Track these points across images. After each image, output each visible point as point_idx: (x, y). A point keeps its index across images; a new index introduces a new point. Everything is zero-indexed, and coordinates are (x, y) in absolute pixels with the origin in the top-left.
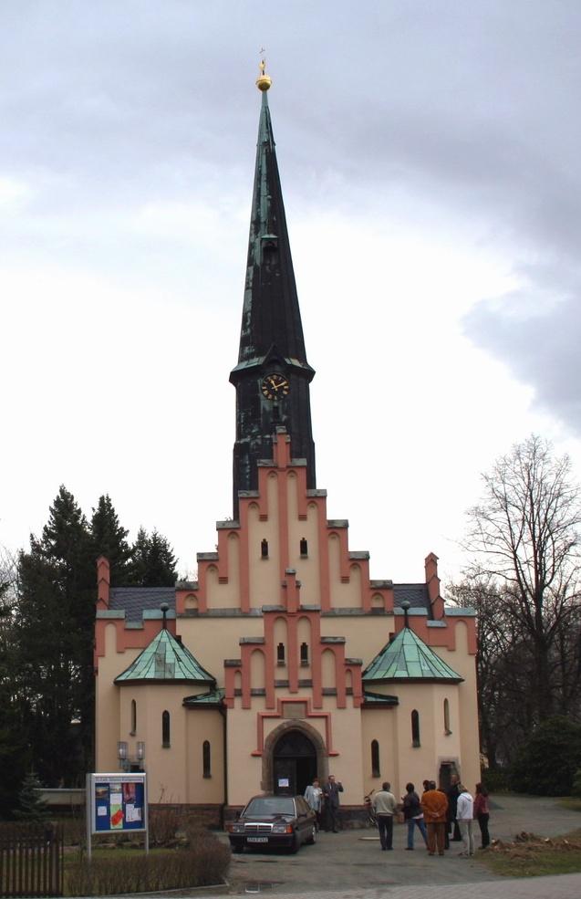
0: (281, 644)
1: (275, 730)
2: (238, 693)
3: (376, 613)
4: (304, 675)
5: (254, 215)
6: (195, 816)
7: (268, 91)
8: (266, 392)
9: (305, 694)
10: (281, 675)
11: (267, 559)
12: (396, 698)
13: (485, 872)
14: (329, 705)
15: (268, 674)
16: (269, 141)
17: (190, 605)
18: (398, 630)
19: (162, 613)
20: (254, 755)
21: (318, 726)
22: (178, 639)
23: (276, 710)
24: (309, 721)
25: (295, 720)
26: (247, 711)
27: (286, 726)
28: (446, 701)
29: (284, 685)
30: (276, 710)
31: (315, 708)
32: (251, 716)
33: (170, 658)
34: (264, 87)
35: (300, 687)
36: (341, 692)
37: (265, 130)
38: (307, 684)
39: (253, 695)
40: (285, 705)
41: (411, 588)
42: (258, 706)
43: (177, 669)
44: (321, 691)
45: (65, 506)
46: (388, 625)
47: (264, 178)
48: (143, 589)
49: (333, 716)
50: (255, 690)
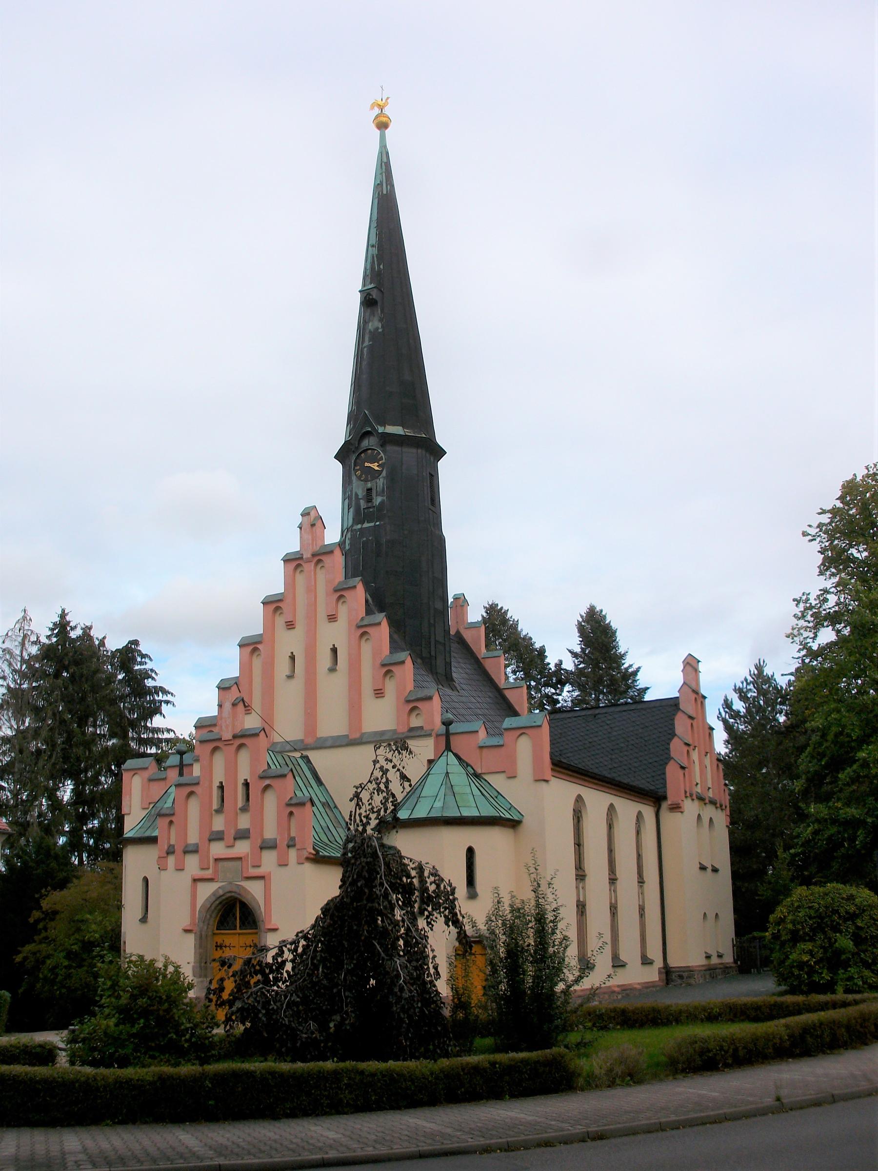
0: (221, 783)
1: (210, 897)
4: (244, 822)
7: (387, 132)
9: (242, 848)
10: (218, 823)
14: (269, 859)
20: (187, 931)
21: (255, 891)
23: (210, 871)
25: (231, 883)
27: (221, 892)
28: (470, 852)
29: (218, 837)
30: (210, 871)
31: (254, 867)
32: (185, 878)
34: (382, 126)
35: (235, 839)
36: (282, 844)
38: (243, 835)
40: (221, 864)
41: (658, 704)
42: (192, 863)
44: (259, 842)
45: (485, 607)
49: (273, 878)
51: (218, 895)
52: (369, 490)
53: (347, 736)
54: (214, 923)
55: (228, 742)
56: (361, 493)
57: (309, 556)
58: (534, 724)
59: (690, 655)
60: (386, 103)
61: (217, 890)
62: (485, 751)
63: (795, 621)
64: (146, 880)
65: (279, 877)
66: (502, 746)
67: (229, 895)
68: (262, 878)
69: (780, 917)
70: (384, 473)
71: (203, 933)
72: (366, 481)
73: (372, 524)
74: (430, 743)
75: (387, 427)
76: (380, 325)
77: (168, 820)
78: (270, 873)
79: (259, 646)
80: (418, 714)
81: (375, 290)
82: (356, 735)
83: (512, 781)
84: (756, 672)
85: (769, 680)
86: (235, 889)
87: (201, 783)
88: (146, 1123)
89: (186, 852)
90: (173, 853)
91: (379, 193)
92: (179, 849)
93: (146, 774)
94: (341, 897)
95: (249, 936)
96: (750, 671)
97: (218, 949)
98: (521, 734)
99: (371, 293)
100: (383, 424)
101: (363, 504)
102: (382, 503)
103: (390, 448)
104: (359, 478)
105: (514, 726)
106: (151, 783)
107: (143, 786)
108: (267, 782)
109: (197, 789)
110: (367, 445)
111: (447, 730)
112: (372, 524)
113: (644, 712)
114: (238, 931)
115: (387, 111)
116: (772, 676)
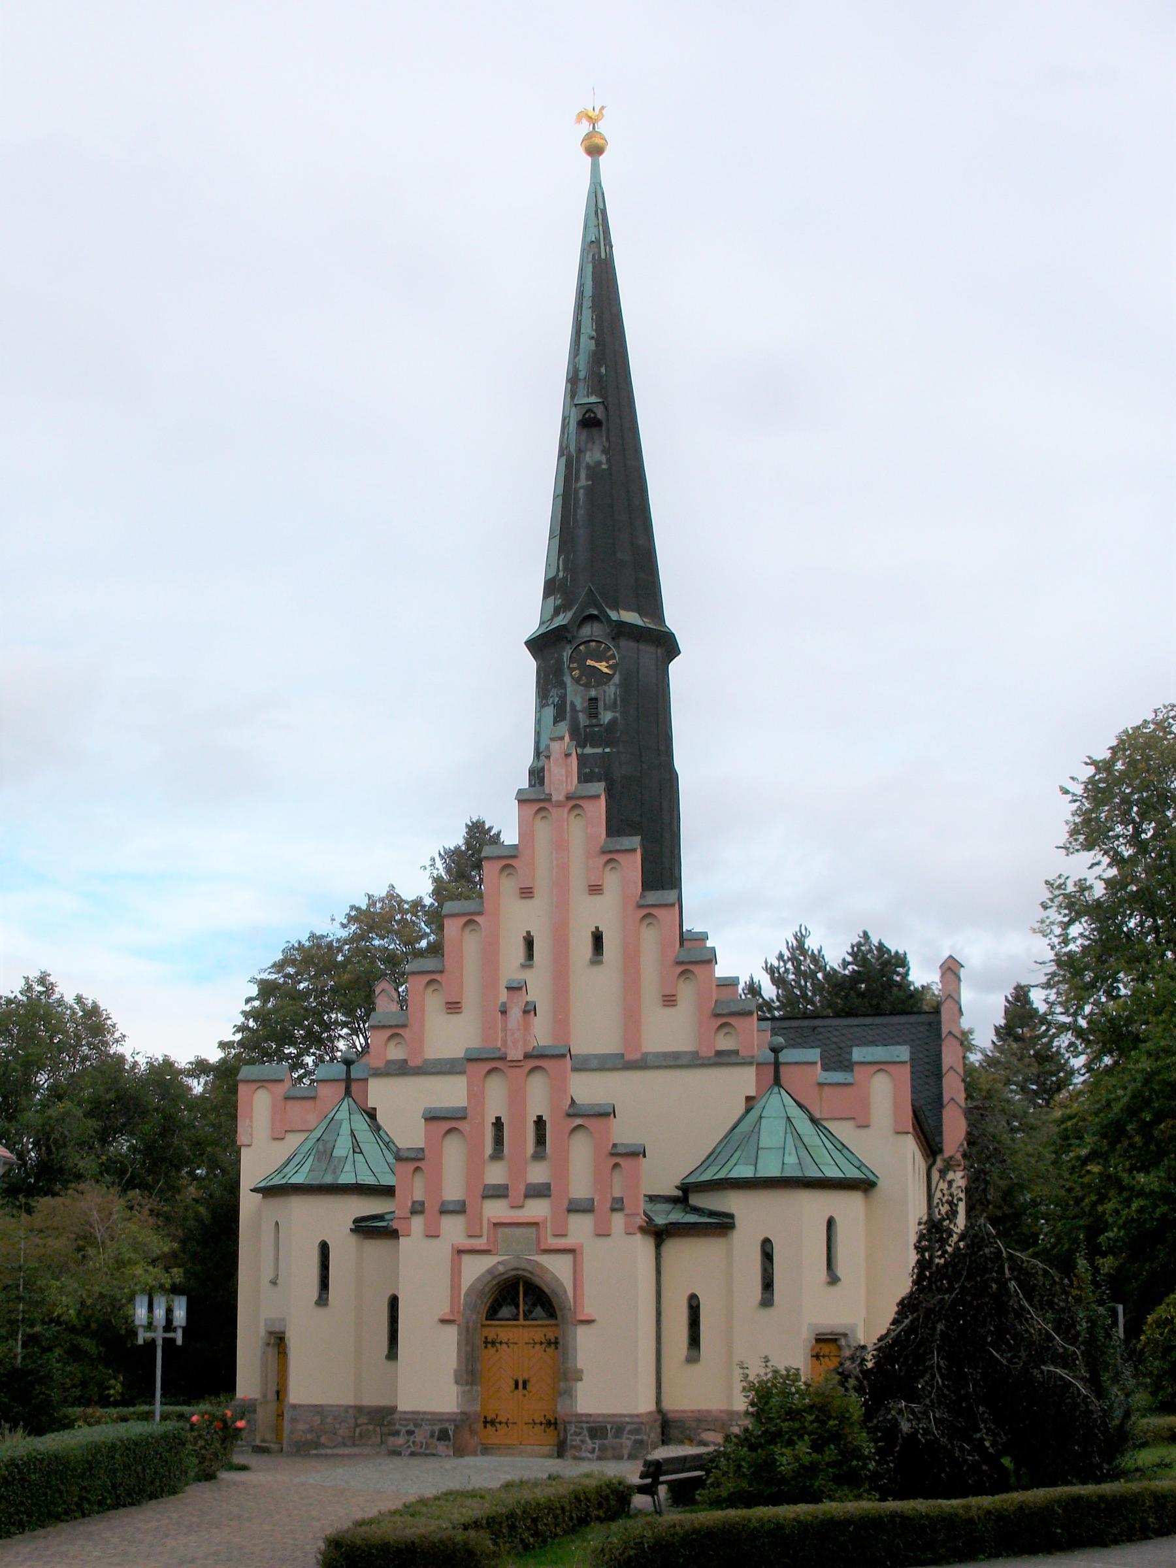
0: (498, 1119)
1: (483, 1275)
2: (417, 1209)
3: (724, 1059)
4: (538, 1174)
5: (571, 366)
6: (371, 1427)
7: (601, 158)
8: (576, 673)
9: (537, 1209)
10: (496, 1174)
11: (600, 962)
12: (731, 1216)
13: (378, 1453)
14: (580, 1228)
15: (473, 1170)
16: (598, 241)
17: (395, 1053)
18: (763, 1090)
19: (345, 1067)
20: (444, 1321)
21: (558, 1269)
22: (372, 1115)
23: (484, 1240)
24: (547, 1261)
26: (434, 1241)
27: (501, 1269)
28: (830, 1223)
29: (498, 1192)
30: (484, 1240)
31: (556, 1236)
32: (441, 1249)
33: (343, 1147)
34: (595, 150)
35: (526, 1196)
37: (593, 221)
38: (539, 1192)
39: (445, 1211)
40: (501, 1230)
42: (453, 1229)
43: (348, 1167)
46: (745, 1080)
47: (587, 303)
48: (868, 1020)
50: (449, 1202)
51: (497, 1273)
52: (593, 701)
53: (622, 1055)
54: (483, 1310)
55: (515, 1064)
56: (580, 703)
57: (562, 798)
58: (898, 1059)
59: (951, 957)
60: (601, 115)
61: (494, 1267)
62: (826, 1088)
63: (1043, 914)
64: (324, 1248)
65: (595, 1253)
66: (850, 1084)
67: (514, 1273)
68: (571, 1251)
69: (1167, 1318)
70: (616, 679)
71: (471, 1324)
72: (587, 686)
73: (599, 750)
74: (750, 1074)
75: (622, 612)
76: (604, 459)
77: (411, 1166)
78: (582, 1246)
79: (477, 919)
80: (727, 1033)
81: (601, 406)
82: (635, 1056)
83: (863, 1132)
84: (795, 943)
85: (816, 959)
86: (524, 1265)
87: (469, 1118)
88: (1008, 1556)
89: (443, 1212)
90: (422, 1212)
91: (594, 255)
92: (432, 1208)
93: (281, 1090)
94: (912, 1293)
95: (539, 1329)
96: (788, 943)
97: (489, 1346)
98: (879, 1071)
99: (595, 410)
100: (616, 607)
101: (583, 719)
102: (613, 721)
103: (623, 642)
104: (577, 681)
105: (869, 1059)
106: (290, 1104)
107: (274, 1106)
108: (579, 1121)
109: (463, 1126)
110: (589, 633)
111: (776, 1058)
112: (599, 750)
113: (885, 1030)
114: (521, 1322)
115: (601, 127)
116: (820, 951)
